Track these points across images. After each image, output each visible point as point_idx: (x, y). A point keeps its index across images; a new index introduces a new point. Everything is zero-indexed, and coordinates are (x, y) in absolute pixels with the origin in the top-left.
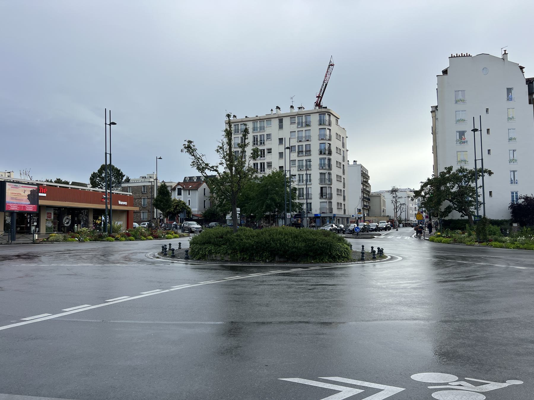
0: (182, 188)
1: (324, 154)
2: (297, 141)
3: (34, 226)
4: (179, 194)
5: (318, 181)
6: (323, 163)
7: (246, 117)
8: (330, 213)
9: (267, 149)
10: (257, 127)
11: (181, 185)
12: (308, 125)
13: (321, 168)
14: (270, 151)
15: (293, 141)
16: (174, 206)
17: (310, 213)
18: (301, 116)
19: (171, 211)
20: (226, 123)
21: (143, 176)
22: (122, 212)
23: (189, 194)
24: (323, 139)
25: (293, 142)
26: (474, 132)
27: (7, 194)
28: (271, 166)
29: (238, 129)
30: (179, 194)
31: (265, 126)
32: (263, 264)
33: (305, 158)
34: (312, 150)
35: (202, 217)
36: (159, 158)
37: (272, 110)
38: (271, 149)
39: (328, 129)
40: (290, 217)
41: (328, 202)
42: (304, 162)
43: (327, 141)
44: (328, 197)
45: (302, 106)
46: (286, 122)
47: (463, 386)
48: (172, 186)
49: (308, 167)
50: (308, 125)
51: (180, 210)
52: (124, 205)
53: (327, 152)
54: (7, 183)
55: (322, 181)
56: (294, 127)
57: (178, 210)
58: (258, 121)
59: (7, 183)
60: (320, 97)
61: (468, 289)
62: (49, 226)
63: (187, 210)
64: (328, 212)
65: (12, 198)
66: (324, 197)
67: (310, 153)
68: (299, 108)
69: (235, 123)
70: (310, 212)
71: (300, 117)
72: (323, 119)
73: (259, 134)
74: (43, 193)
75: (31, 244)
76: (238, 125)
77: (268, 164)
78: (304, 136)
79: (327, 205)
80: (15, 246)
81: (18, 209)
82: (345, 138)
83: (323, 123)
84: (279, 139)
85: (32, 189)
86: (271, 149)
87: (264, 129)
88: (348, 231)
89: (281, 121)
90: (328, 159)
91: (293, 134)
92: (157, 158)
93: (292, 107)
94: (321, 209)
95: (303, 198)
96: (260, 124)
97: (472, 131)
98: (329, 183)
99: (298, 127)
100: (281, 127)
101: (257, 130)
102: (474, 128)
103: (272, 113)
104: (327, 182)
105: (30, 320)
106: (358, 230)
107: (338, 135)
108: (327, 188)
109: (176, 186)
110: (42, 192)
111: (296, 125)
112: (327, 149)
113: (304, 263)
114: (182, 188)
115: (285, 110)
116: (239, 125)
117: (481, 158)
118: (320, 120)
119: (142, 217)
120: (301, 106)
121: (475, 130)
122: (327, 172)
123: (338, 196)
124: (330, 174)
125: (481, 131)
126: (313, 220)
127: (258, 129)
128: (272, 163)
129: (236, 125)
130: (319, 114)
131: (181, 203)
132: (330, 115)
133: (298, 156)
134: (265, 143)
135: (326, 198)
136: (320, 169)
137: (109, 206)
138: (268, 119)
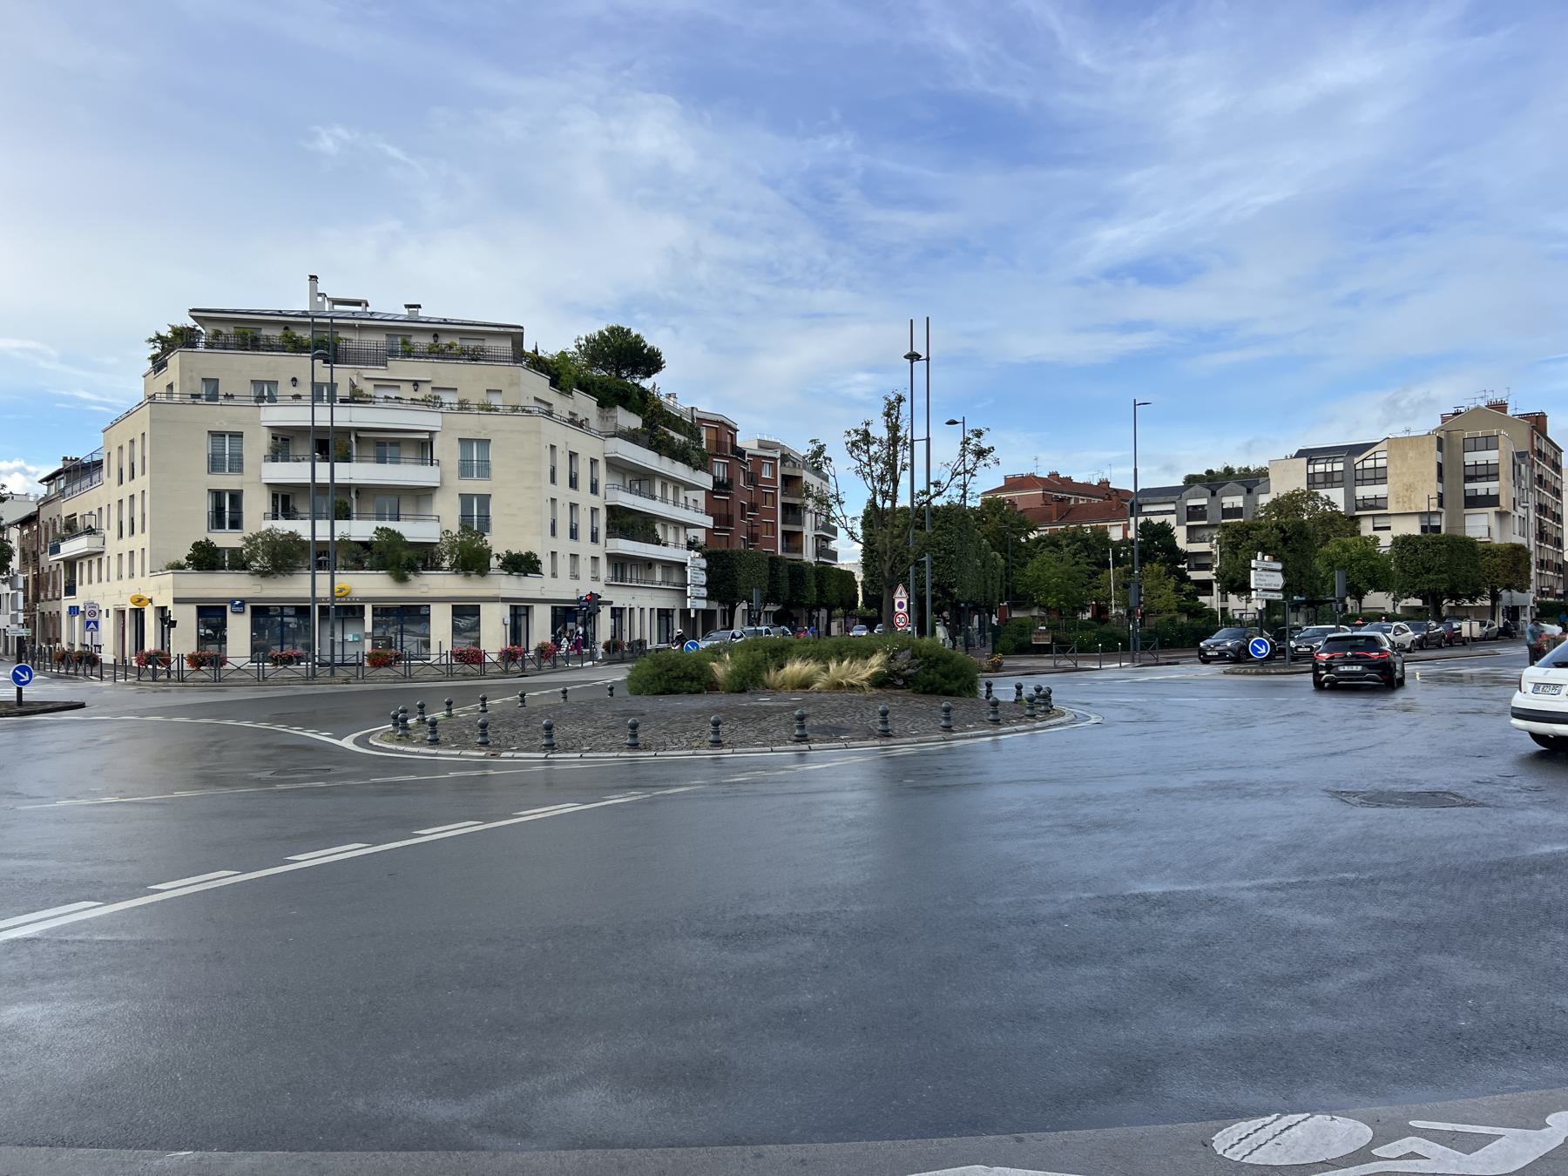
26: (912, 363)
47: (1427, 1158)
61: (77, 867)
92: (1135, 405)
97: (906, 357)
105: (430, 834)
106: (1263, 651)
117: (926, 437)
121: (913, 357)
125: (928, 359)
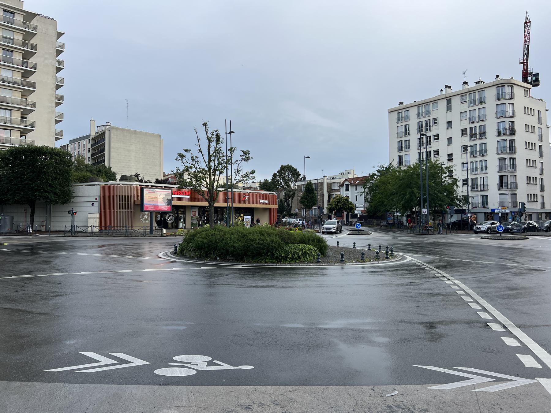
0: (349, 184)
1: (504, 134)
2: (468, 122)
3: (181, 222)
4: (347, 190)
5: (496, 169)
6: (483, 149)
7: (401, 103)
8: (514, 207)
9: (433, 135)
10: (422, 112)
11: (348, 181)
12: (481, 102)
13: (500, 152)
14: (437, 137)
15: (464, 124)
16: (335, 203)
17: (486, 207)
18: (483, 91)
19: (333, 207)
20: (389, 112)
21: (342, 172)
22: (265, 209)
23: (356, 190)
24: (502, 117)
25: (464, 124)
27: (144, 198)
28: (439, 154)
29: (402, 117)
30: (347, 190)
31: (431, 110)
32: (205, 262)
33: (478, 142)
34: (487, 131)
35: (366, 213)
36: (307, 157)
37: (442, 90)
38: (438, 135)
39: (509, 103)
40: (426, 214)
41: (510, 194)
42: (478, 146)
43: (508, 118)
44: (509, 187)
45: (481, 80)
46: (455, 101)
48: (340, 182)
49: (483, 152)
50: (481, 102)
51: (342, 206)
52: (266, 203)
53: (508, 132)
54: (145, 189)
55: (501, 168)
56: (465, 107)
57: (339, 207)
58: (423, 105)
59: (145, 189)
60: (525, 63)
62: (194, 222)
63: (348, 206)
64: (510, 206)
65: (149, 201)
66: (504, 188)
67: (485, 135)
68: (477, 83)
69: (398, 111)
70: (487, 206)
71: (473, 94)
72: (502, 93)
73: (424, 120)
74: (187, 195)
75: (159, 237)
76: (402, 112)
77: (435, 152)
78: (477, 115)
79: (509, 198)
80: (115, 239)
81: (154, 209)
82: (543, 111)
83: (502, 97)
84: (447, 122)
85: (166, 193)
86: (438, 135)
87: (430, 113)
88: (516, 230)
89: (449, 101)
90: (510, 141)
91: (464, 114)
93: (465, 83)
94: (500, 202)
95: (477, 190)
96: (426, 108)
98: (512, 170)
99: (469, 106)
100: (449, 108)
101: (422, 115)
102: (231, 130)
103: (441, 93)
104: (508, 169)
106: (501, 229)
107: (529, 109)
108: (509, 177)
109: (344, 182)
110: (184, 195)
111: (467, 104)
112: (508, 128)
113: (239, 263)
114: (349, 184)
115: (457, 88)
116: (403, 112)
118: (498, 94)
119: (314, 213)
120: (479, 81)
122: (509, 156)
123: (529, 185)
124: (513, 159)
126: (491, 217)
127: (424, 114)
128: (439, 151)
129: (400, 113)
130: (508, 85)
131: (343, 199)
132: (512, 87)
133: (470, 140)
134: (432, 128)
135: (508, 188)
136: (498, 154)
137: (231, 204)
138: (435, 101)
